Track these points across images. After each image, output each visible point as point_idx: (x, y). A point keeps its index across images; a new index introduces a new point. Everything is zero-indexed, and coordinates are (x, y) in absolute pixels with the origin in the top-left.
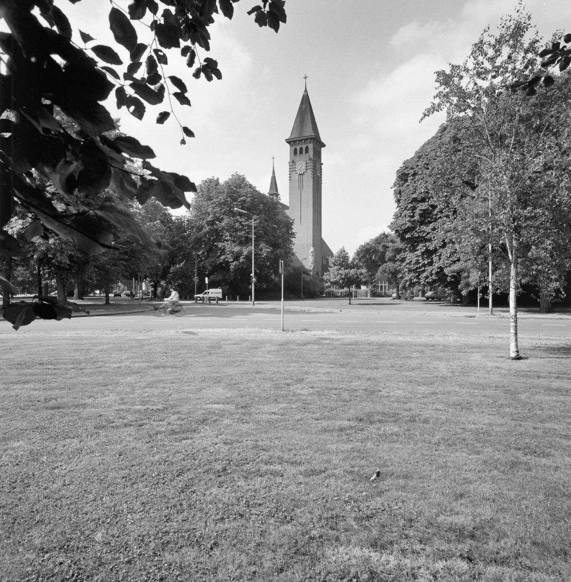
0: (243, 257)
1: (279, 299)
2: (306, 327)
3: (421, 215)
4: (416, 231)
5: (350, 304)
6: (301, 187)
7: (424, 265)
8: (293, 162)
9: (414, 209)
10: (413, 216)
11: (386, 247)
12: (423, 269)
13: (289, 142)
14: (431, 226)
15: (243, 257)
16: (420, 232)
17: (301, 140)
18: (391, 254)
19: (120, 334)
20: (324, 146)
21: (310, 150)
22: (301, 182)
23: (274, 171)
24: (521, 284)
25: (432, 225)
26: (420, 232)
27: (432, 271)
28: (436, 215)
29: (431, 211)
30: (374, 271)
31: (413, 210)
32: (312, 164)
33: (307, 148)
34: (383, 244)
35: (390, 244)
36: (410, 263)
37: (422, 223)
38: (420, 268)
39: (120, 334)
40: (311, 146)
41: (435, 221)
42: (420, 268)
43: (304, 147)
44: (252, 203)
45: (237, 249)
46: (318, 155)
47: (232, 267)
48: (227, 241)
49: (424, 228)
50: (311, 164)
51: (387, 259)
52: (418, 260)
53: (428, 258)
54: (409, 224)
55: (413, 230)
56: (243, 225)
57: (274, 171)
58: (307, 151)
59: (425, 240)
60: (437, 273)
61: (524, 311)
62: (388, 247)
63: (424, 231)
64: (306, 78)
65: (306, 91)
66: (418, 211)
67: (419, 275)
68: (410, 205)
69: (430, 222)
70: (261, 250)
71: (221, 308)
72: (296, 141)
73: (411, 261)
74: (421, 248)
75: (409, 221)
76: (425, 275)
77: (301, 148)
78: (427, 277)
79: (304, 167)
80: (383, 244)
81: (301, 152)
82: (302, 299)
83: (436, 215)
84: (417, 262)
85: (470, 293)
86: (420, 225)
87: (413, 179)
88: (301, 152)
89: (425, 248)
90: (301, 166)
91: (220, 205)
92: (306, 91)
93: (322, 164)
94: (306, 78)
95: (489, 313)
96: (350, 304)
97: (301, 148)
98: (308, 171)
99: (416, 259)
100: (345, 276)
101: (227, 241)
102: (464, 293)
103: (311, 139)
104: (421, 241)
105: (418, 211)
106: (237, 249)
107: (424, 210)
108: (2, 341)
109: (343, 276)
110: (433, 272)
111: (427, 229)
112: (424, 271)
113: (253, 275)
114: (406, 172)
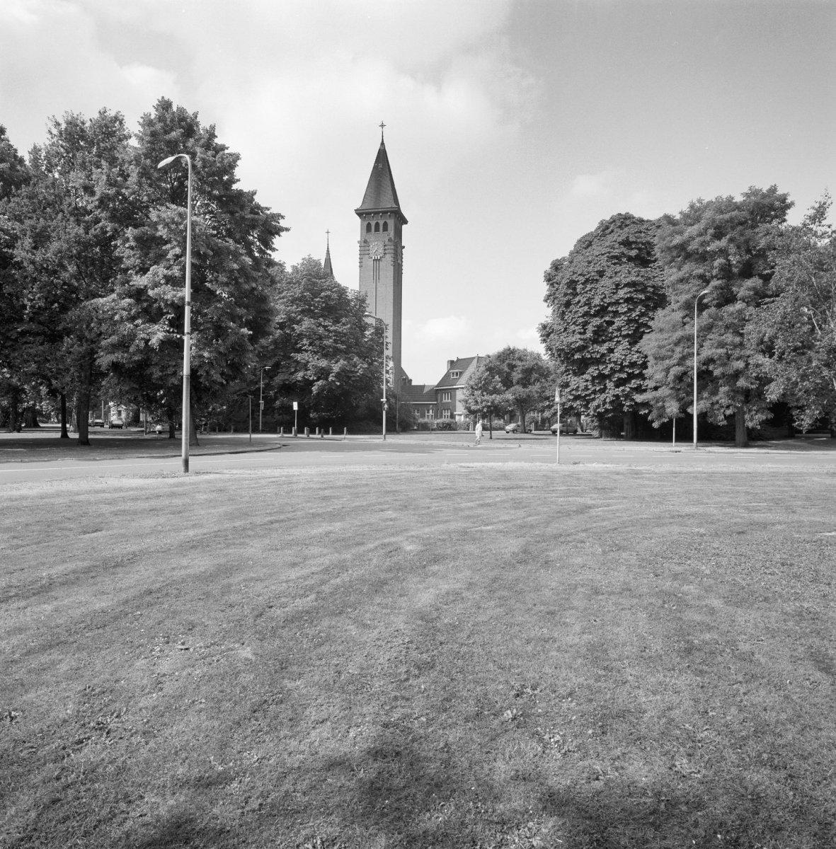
0: (333, 374)
1: (380, 432)
2: (576, 461)
3: (595, 332)
4: (588, 352)
5: (491, 438)
6: (376, 278)
7: (594, 392)
8: (365, 242)
9: (585, 324)
10: (584, 333)
11: (512, 367)
12: (593, 396)
13: (360, 213)
14: (606, 345)
15: (333, 374)
16: (593, 353)
17: (376, 213)
18: (520, 376)
19: (391, 468)
20: (405, 222)
21: (389, 228)
22: (376, 270)
23: (328, 251)
24: (725, 416)
25: (607, 343)
26: (593, 353)
27: (605, 399)
28: (612, 333)
29: (607, 328)
30: (508, 394)
31: (584, 326)
32: (392, 247)
33: (385, 225)
34: (507, 362)
35: (519, 363)
36: (577, 389)
37: (595, 341)
38: (589, 395)
39: (391, 468)
40: (391, 223)
41: (610, 340)
42: (589, 395)
43: (381, 223)
44: (339, 300)
45: (323, 363)
46: (398, 233)
47: (315, 389)
48: (306, 351)
49: (596, 347)
50: (391, 247)
51: (514, 381)
52: (587, 386)
53: (599, 383)
54: (581, 343)
55: (584, 350)
56: (328, 331)
57: (328, 251)
58: (385, 229)
59: (597, 362)
60: (612, 402)
61: (730, 446)
62: (515, 366)
63: (598, 352)
64: (382, 126)
65: (383, 144)
66: (590, 328)
67: (588, 403)
68: (581, 320)
69: (604, 342)
70: (355, 366)
71: (332, 444)
72: (371, 213)
73: (578, 387)
74: (592, 371)
75: (581, 339)
76: (595, 403)
77: (377, 224)
78: (598, 407)
79: (381, 251)
80: (507, 362)
81: (377, 229)
82: (398, 433)
83: (612, 333)
84: (586, 388)
85: (663, 425)
86: (593, 344)
87: (583, 289)
88: (377, 229)
89: (597, 372)
90: (377, 248)
91: (294, 301)
92: (383, 144)
93: (404, 247)
94: (382, 126)
95: (179, 462)
96: (491, 438)
97: (377, 224)
98: (387, 256)
99: (585, 384)
100: (492, 403)
101: (306, 351)
102: (656, 425)
103: (392, 212)
104: (593, 364)
105: (590, 328)
106: (323, 363)
107: (597, 326)
108: (1, 497)
109: (489, 404)
110: (608, 400)
111: (603, 349)
112: (594, 399)
113: (384, 400)
114: (574, 277)
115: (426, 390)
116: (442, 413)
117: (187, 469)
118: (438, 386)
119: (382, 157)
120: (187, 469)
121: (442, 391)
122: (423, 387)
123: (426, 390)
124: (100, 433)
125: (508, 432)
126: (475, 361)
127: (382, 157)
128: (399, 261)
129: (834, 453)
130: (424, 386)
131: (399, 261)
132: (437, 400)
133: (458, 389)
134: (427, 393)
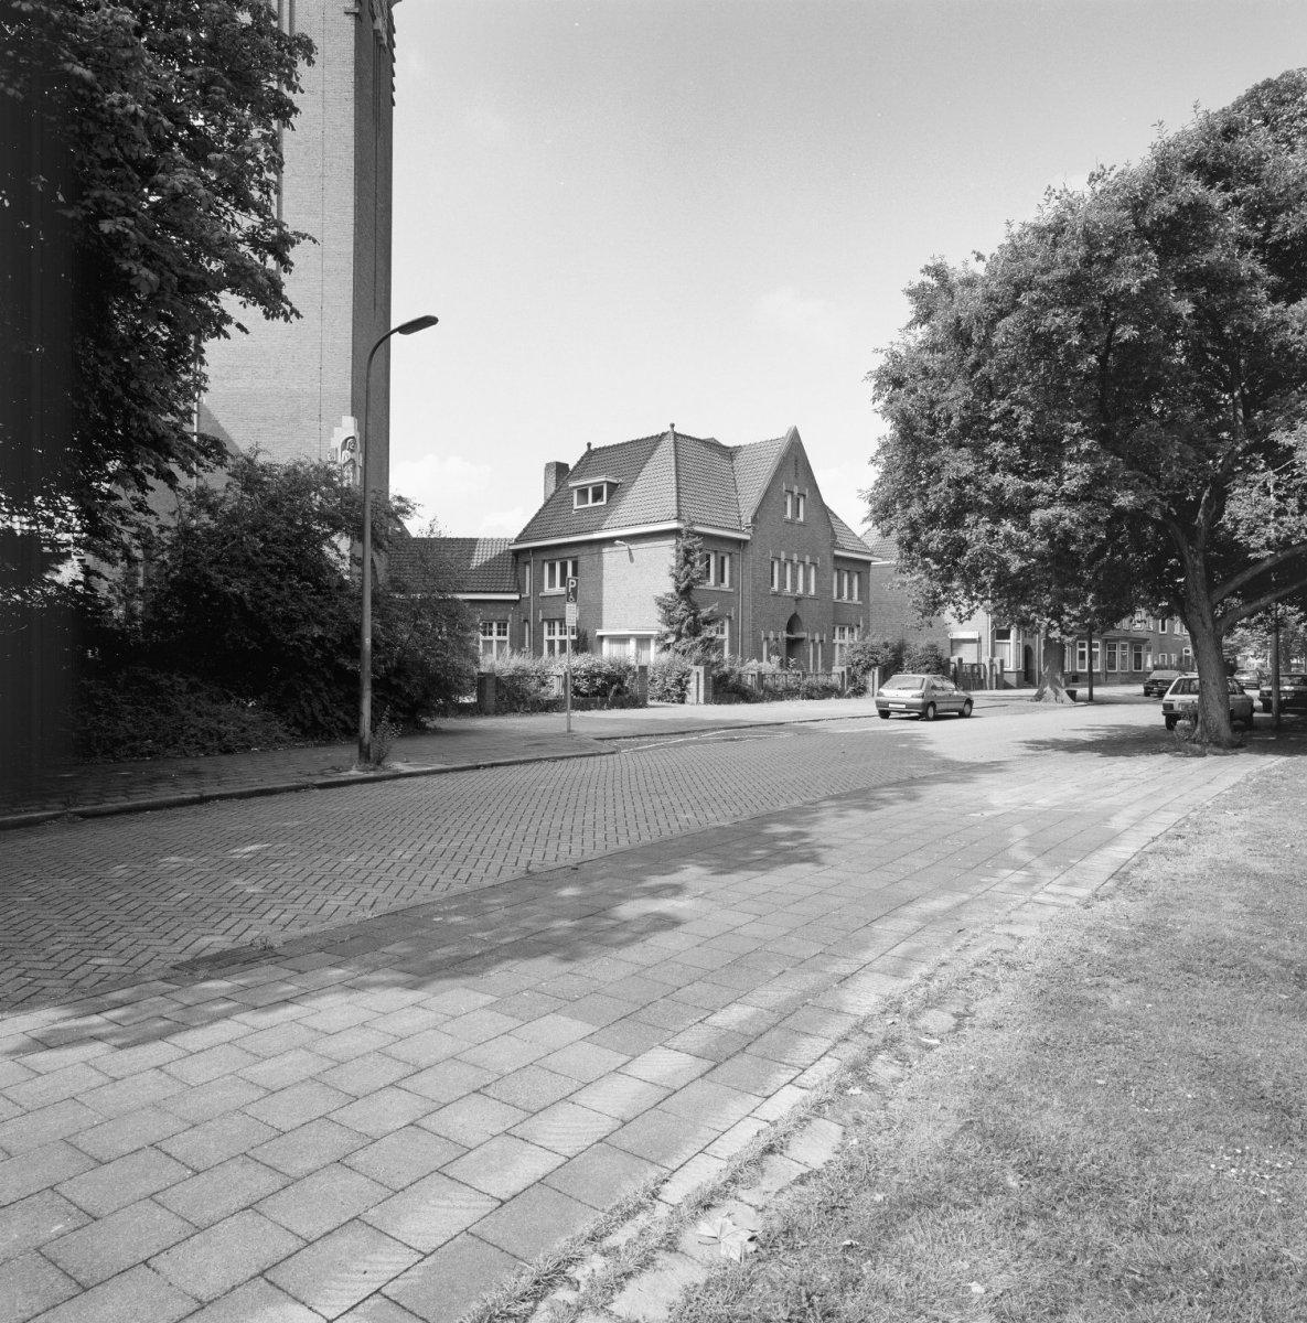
115: (478, 560)
116: (538, 634)
117: (632, 560)
118: (518, 541)
119: (247, 333)
120: (632, 560)
121: (553, 552)
122: (471, 543)
123: (478, 560)
124: (815, 663)
125: (885, 714)
126: (667, 446)
127: (247, 333)
128: (380, 24)
129: (1304, 760)
130: (473, 542)
131: (380, 24)
132: (519, 589)
133: (610, 541)
134: (487, 565)
